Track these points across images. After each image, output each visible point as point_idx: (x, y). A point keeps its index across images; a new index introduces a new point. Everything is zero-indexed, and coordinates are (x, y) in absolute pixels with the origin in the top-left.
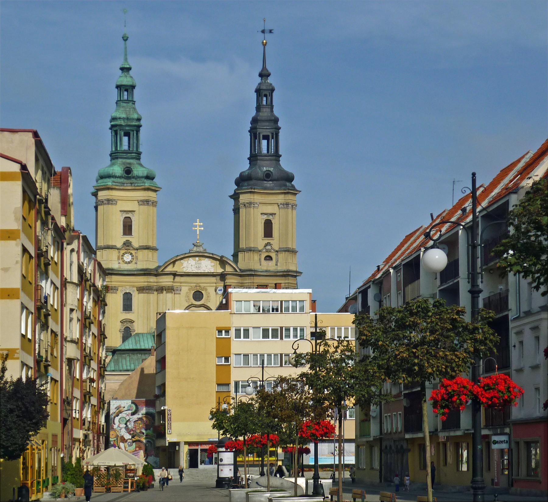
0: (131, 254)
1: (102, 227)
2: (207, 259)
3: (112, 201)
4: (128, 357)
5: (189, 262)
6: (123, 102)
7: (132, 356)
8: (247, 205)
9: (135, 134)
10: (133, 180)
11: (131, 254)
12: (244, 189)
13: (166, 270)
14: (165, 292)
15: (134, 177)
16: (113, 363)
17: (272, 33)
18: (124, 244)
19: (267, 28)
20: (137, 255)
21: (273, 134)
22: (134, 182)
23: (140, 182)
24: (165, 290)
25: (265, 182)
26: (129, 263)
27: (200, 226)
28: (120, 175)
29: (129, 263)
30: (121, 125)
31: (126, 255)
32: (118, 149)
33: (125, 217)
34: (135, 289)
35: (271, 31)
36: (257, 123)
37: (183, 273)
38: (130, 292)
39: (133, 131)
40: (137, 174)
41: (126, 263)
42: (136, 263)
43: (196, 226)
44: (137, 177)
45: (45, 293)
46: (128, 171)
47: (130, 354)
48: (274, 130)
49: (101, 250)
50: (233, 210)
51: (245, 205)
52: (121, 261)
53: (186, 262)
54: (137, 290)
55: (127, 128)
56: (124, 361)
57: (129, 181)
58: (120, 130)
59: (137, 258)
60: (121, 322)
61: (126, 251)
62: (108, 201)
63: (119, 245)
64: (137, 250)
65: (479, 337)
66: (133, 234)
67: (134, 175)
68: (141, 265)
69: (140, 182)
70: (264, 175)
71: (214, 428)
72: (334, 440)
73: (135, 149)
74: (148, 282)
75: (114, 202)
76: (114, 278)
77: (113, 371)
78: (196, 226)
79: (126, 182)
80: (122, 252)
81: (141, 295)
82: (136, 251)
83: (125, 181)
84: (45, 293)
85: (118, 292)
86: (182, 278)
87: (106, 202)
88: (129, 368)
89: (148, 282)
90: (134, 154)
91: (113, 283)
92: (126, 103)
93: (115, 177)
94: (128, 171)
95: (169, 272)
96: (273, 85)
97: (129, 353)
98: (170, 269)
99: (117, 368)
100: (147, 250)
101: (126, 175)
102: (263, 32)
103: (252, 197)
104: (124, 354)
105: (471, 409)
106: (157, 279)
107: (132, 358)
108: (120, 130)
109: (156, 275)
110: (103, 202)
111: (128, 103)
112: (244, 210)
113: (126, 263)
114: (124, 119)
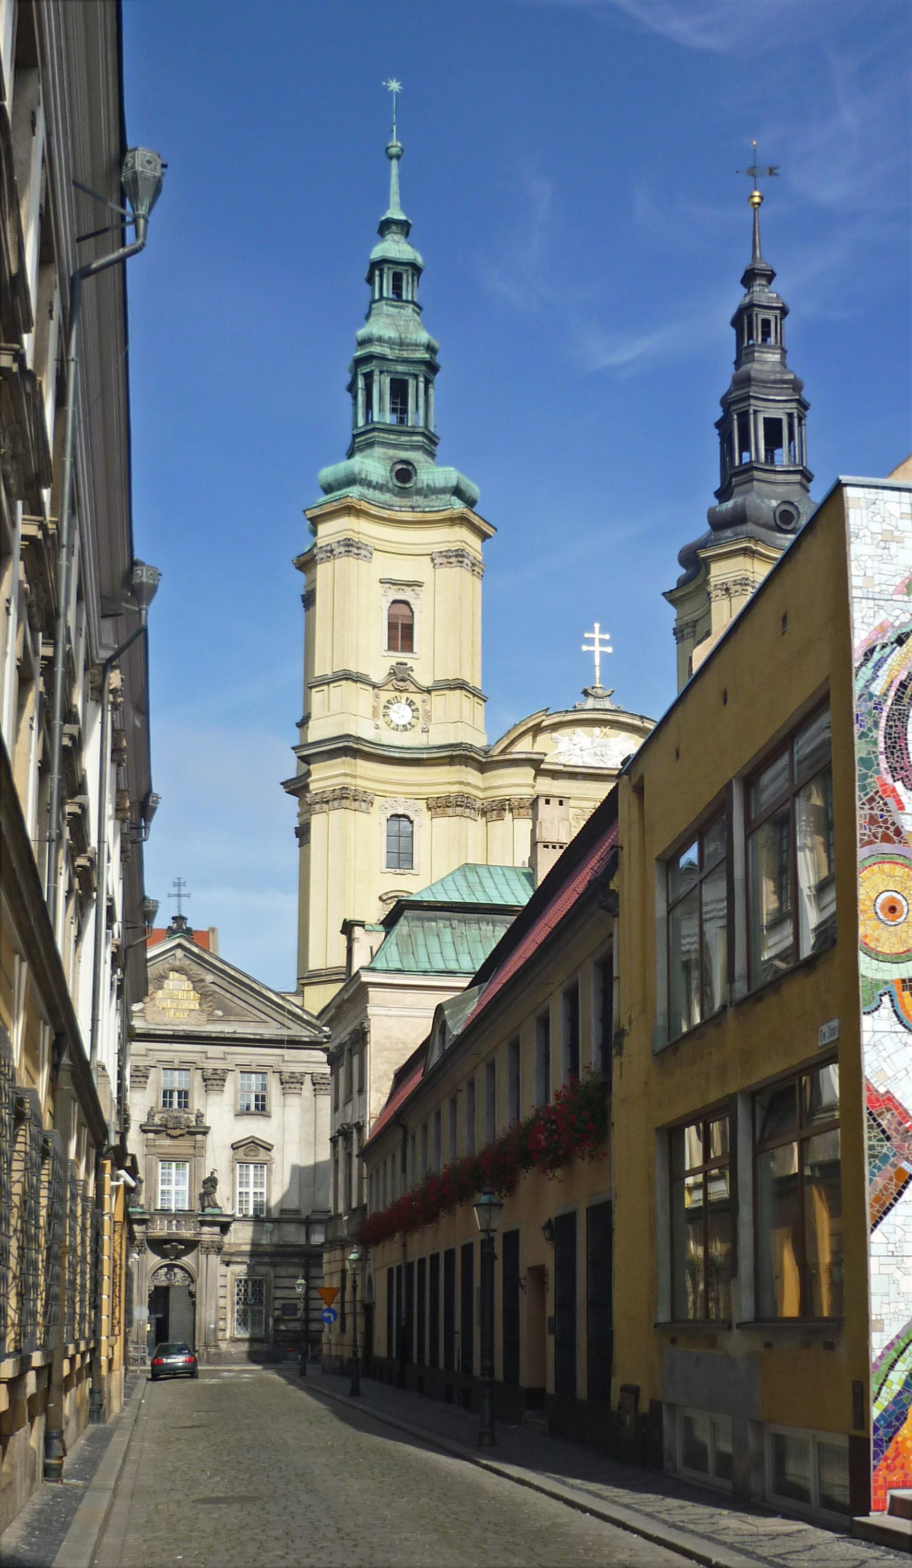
1: (330, 622)
2: (624, 734)
3: (358, 548)
4: (448, 930)
5: (576, 739)
6: (387, 304)
7: (461, 928)
8: (733, 589)
9: (422, 385)
10: (418, 500)
12: (727, 544)
13: (515, 749)
15: (419, 492)
16: (394, 948)
17: (776, 174)
18: (393, 673)
20: (428, 708)
21: (790, 416)
22: (420, 503)
23: (437, 504)
24: (511, 810)
25: (779, 535)
26: (405, 728)
27: (603, 642)
28: (380, 481)
30: (383, 358)
31: (395, 707)
32: (376, 419)
33: (395, 602)
34: (423, 804)
35: (772, 172)
36: (251, 1251)
37: (561, 768)
39: (416, 377)
40: (431, 483)
43: (591, 642)
44: (431, 491)
46: (405, 473)
47: (455, 923)
48: (794, 405)
49: (325, 687)
50: (676, 632)
51: (727, 590)
52: (381, 722)
53: (567, 739)
54: (429, 809)
55: (401, 368)
56: (433, 943)
57: (406, 502)
58: (381, 372)
59: (428, 716)
60: (380, 898)
61: (397, 694)
62: (348, 545)
63: (378, 676)
64: (429, 691)
66: (416, 648)
67: (419, 485)
68: (441, 735)
69: (437, 504)
70: (777, 516)
73: (421, 423)
74: (461, 783)
75: (363, 552)
76: (363, 767)
77: (399, 971)
78: (591, 642)
79: (398, 504)
80: (385, 696)
81: (442, 823)
82: (425, 696)
83: (396, 500)
85: (372, 810)
86: (555, 783)
87: (342, 549)
88: (453, 966)
89: (461, 783)
90: (420, 438)
91: (359, 782)
92: (397, 307)
93: (369, 484)
94: (405, 473)
95: (524, 756)
97: (449, 919)
98: (524, 747)
99: (410, 964)
100: (458, 691)
101: (399, 484)
103: (749, 567)
104: (430, 920)
105: (847, 1465)
106: (484, 779)
107: (462, 936)
108: (381, 372)
109: (483, 768)
110: (332, 551)
111: (401, 307)
112: (726, 603)
114: (390, 342)
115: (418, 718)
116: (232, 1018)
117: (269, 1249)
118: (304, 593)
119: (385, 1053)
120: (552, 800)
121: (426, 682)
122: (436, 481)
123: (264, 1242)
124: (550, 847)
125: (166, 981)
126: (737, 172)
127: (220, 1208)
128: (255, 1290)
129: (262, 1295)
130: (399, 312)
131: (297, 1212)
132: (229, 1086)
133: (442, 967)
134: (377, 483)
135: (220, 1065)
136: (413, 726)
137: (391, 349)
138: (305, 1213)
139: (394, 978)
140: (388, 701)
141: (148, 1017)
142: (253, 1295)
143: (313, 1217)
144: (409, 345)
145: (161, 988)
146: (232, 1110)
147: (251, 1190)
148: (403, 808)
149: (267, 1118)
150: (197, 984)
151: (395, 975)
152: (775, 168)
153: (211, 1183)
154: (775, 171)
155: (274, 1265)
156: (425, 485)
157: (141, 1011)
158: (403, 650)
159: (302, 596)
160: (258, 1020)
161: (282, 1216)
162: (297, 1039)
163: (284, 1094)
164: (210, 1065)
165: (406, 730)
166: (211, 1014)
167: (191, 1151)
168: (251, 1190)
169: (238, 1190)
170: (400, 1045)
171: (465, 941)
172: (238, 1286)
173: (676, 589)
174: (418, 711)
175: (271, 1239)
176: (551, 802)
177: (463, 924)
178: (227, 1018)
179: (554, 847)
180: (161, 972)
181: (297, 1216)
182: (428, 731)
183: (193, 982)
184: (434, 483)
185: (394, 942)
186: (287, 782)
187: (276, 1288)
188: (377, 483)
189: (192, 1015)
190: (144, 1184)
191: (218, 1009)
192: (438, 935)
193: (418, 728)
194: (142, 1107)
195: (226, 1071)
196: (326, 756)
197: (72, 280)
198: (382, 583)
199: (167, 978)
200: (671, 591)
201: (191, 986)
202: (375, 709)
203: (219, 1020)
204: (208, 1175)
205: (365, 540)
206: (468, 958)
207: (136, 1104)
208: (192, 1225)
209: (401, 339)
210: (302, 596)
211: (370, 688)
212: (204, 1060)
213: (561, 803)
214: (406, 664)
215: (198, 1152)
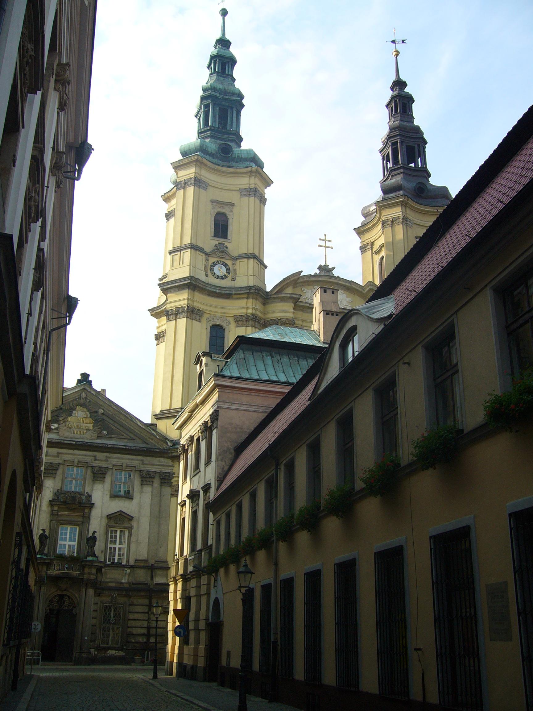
0: (226, 265)
11: (225, 266)
14: (210, 152)
19: (399, 38)
20: (235, 268)
26: (222, 278)
29: (222, 278)
35: (403, 41)
38: (222, 324)
41: (218, 277)
42: (233, 279)
45: (206, 433)
47: (274, 354)
52: (209, 273)
53: (310, 291)
65: (158, 702)
67: (233, 156)
71: (82, 375)
72: (120, 546)
80: (212, 260)
84: (206, 433)
92: (223, 77)
96: (415, 120)
99: (245, 375)
102: (394, 42)
113: (218, 277)
115: (229, 273)
116: (113, 436)
117: (126, 586)
118: (167, 212)
119: (228, 435)
120: (328, 291)
121: (235, 254)
122: (242, 154)
123: (123, 581)
124: (330, 314)
125: (74, 412)
126: (387, 42)
127: (97, 557)
128: (116, 614)
129: (120, 617)
130: (224, 79)
131: (146, 561)
132: (108, 479)
133: (266, 378)
134: (211, 152)
135: (103, 464)
136: (227, 277)
137: (220, 94)
138: (152, 562)
139: (235, 383)
140: (213, 263)
141: (60, 433)
142: (114, 617)
143: (156, 565)
144: (229, 93)
145: (71, 415)
146: (109, 494)
147: (117, 546)
148: (219, 321)
149: (130, 500)
150: (93, 414)
151: (237, 381)
152: (405, 40)
153: (92, 540)
154: (405, 41)
155: (129, 597)
156: (236, 156)
157: (57, 429)
158: (222, 238)
159: (166, 214)
160: (129, 437)
161: (136, 564)
162: (152, 450)
163: (142, 484)
164: (97, 464)
165: (223, 279)
166: (100, 433)
167: (80, 519)
168: (117, 546)
169: (110, 545)
170: (238, 430)
171: (281, 365)
172: (105, 611)
173: (361, 226)
174: (230, 269)
175: (128, 580)
176: (327, 292)
177: (278, 355)
178: (110, 436)
179: (332, 314)
180: (71, 405)
181: (146, 564)
182: (235, 280)
183: (90, 413)
184: (241, 155)
185: (235, 362)
186: (152, 309)
187: (130, 612)
188: (211, 152)
189: (88, 433)
190: (48, 540)
191: (104, 430)
192: (263, 360)
193: (230, 278)
194: (52, 489)
195: (107, 469)
196: (177, 289)
197: (50, 332)
198: (212, 202)
199: (75, 410)
200: (359, 227)
201: (89, 415)
202: (206, 266)
203: (106, 437)
204: (90, 534)
205: (204, 179)
206: (283, 375)
207: (48, 488)
208: (78, 567)
209: (225, 89)
210: (166, 214)
211: (204, 255)
212: (93, 461)
213: (333, 293)
214: (224, 244)
215: (87, 519)
